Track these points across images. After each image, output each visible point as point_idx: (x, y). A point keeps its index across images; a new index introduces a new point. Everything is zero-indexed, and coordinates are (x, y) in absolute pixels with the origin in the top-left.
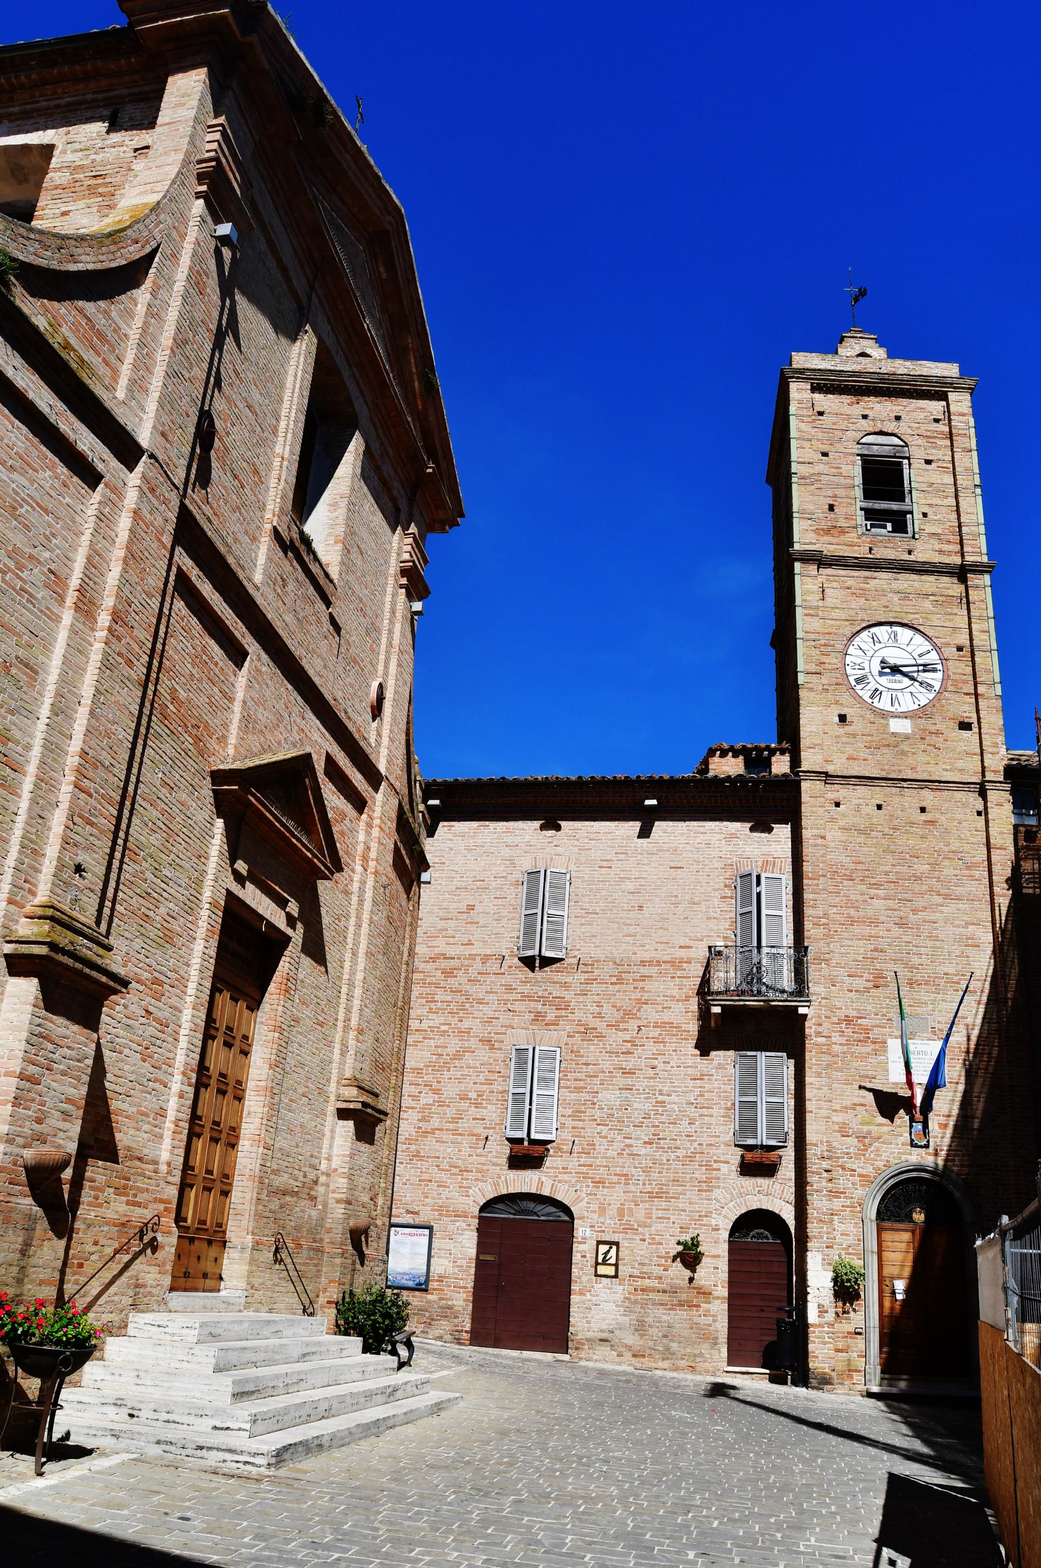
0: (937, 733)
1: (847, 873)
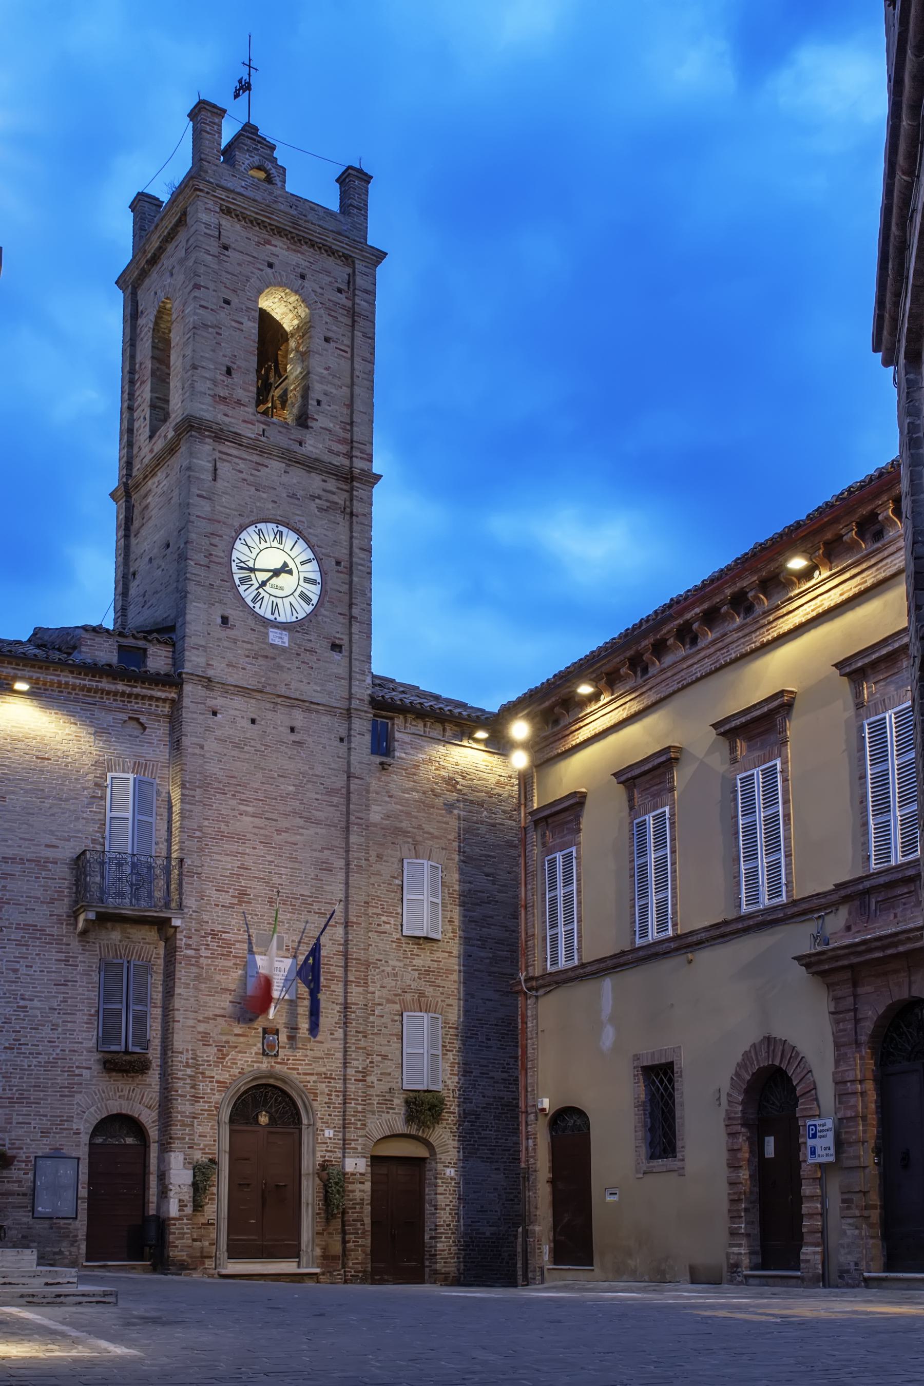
0: (312, 651)
1: (221, 786)
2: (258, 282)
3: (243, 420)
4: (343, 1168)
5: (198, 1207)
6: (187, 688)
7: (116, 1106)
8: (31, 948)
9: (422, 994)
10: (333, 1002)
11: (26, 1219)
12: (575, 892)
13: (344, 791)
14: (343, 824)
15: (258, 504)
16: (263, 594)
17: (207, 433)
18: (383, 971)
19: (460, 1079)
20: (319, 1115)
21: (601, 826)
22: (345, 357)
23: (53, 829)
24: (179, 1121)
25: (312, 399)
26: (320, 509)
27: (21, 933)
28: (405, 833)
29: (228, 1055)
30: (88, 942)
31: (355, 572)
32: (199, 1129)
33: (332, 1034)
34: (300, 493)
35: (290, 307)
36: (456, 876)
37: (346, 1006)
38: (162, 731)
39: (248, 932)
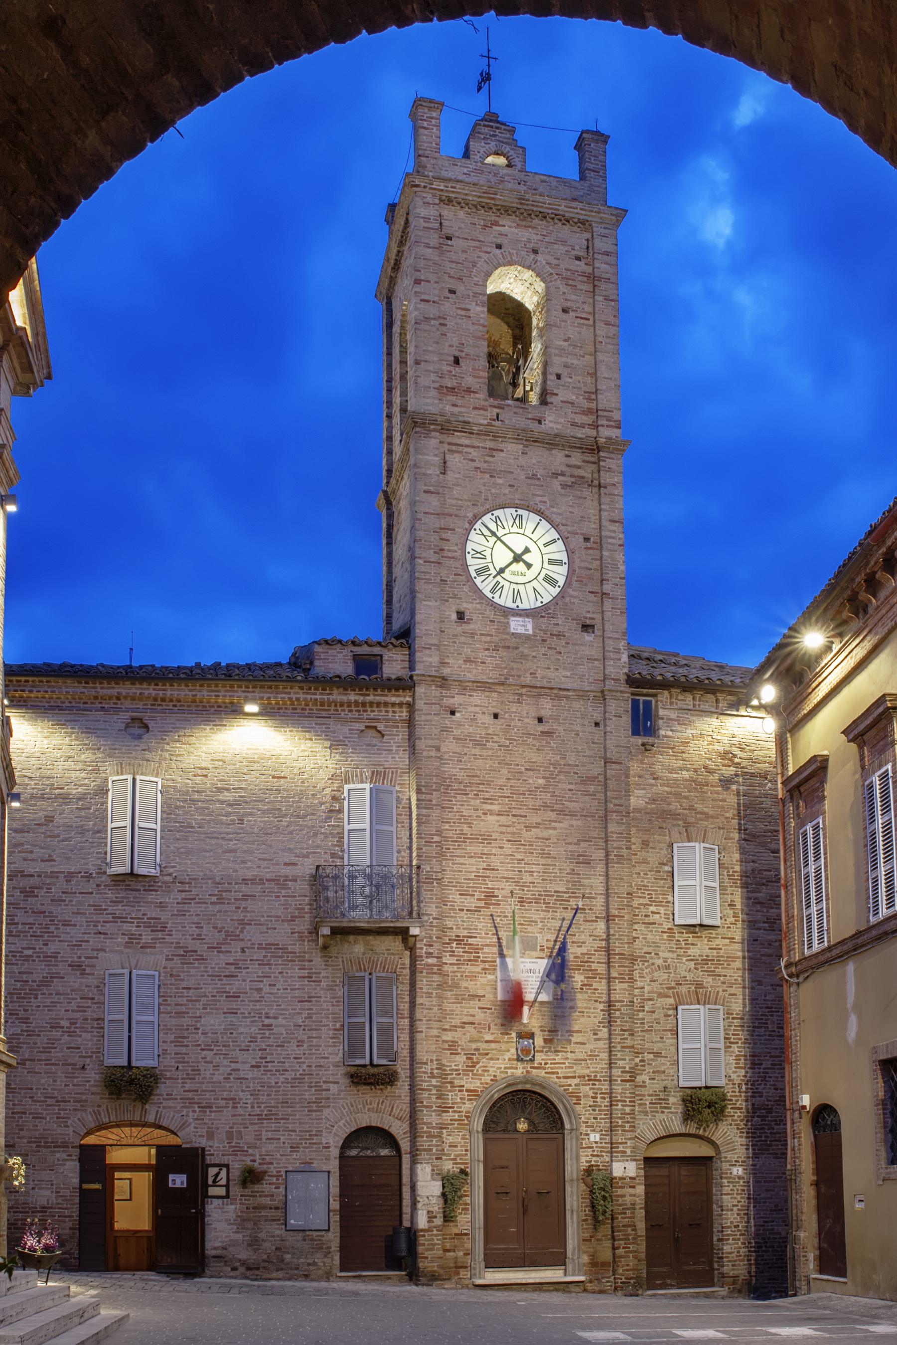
0: (559, 635)
2: (485, 265)
3: (476, 410)
4: (611, 1173)
5: (448, 1218)
6: (420, 690)
7: (366, 1119)
8: (273, 967)
9: (699, 985)
10: (596, 1001)
11: (279, 1231)
12: (823, 867)
13: (601, 778)
14: (602, 813)
15: (493, 491)
16: (502, 582)
17: (432, 427)
18: (653, 964)
19: (747, 1072)
20: (583, 1119)
21: (839, 788)
22: (587, 325)
23: (292, 846)
24: (426, 1132)
25: (551, 374)
26: (564, 486)
27: (263, 952)
28: (674, 815)
29: (478, 1063)
30: (331, 957)
31: (604, 546)
32: (448, 1139)
33: (595, 1034)
34: (540, 473)
35: (527, 284)
36: (737, 856)
37: (610, 1004)
38: (400, 737)
39: (497, 934)
